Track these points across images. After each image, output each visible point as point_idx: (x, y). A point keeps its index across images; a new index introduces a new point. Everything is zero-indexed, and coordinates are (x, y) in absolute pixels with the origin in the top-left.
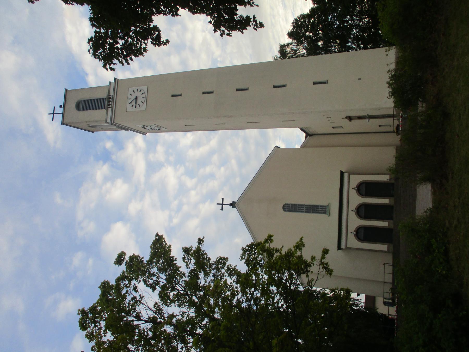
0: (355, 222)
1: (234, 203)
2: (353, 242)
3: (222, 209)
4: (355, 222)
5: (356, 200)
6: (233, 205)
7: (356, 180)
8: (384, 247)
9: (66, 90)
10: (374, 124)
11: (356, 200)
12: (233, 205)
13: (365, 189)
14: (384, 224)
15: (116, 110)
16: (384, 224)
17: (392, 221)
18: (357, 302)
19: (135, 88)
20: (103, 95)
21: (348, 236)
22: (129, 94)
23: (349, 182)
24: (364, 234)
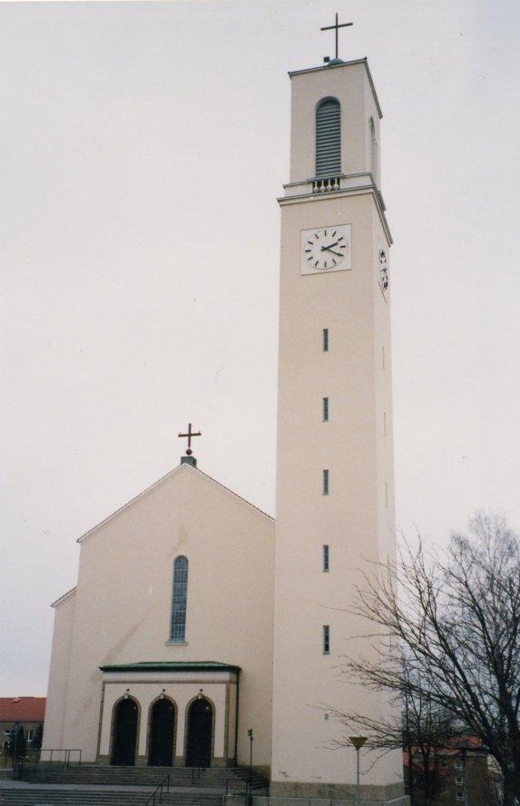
0: (146, 696)
1: (194, 462)
2: (115, 694)
3: (180, 436)
4: (146, 696)
5: (182, 696)
6: (189, 460)
7: (217, 694)
8: (106, 750)
9: (364, 61)
10: (231, 748)
11: (182, 696)
12: (189, 460)
13: (201, 710)
14: (142, 748)
15: (359, 197)
16: (142, 748)
17: (146, 761)
18: (492, 544)
19: (349, 242)
20: (350, 159)
21: (122, 685)
22: (334, 229)
23: (213, 682)
24: (126, 710)
